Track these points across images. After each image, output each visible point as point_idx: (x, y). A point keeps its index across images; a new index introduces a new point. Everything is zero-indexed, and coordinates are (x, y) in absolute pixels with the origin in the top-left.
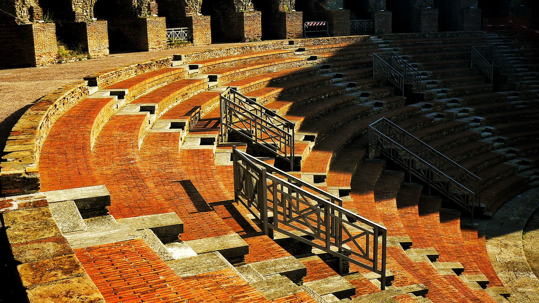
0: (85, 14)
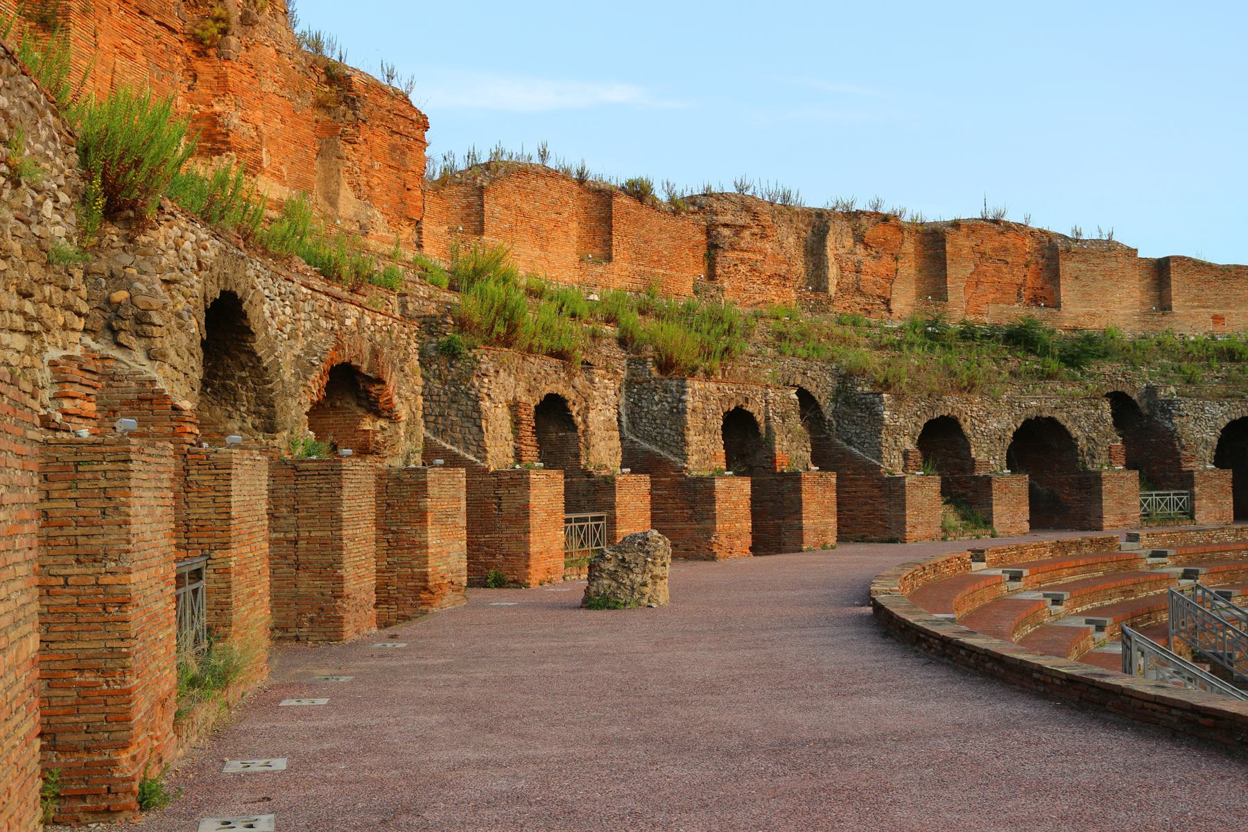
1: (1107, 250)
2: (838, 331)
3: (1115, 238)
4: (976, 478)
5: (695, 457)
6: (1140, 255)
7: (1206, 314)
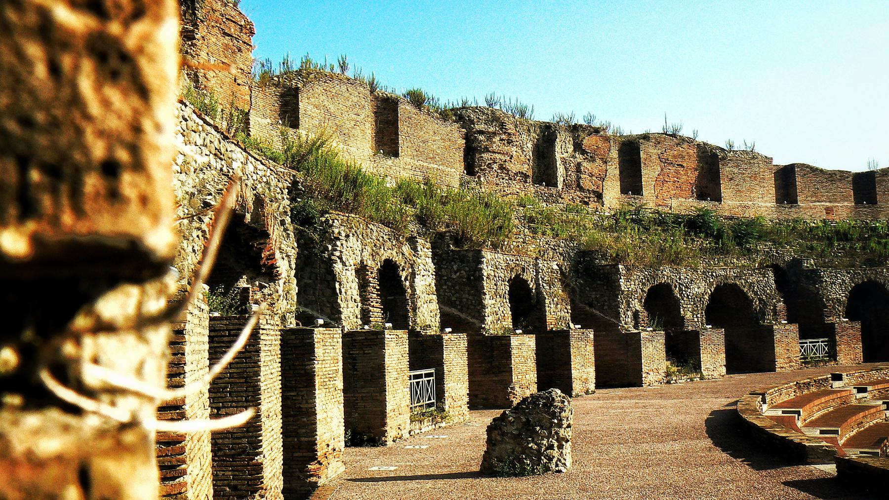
0: (696, 320)
1: (751, 157)
3: (756, 150)
4: (688, 332)
6: (774, 163)
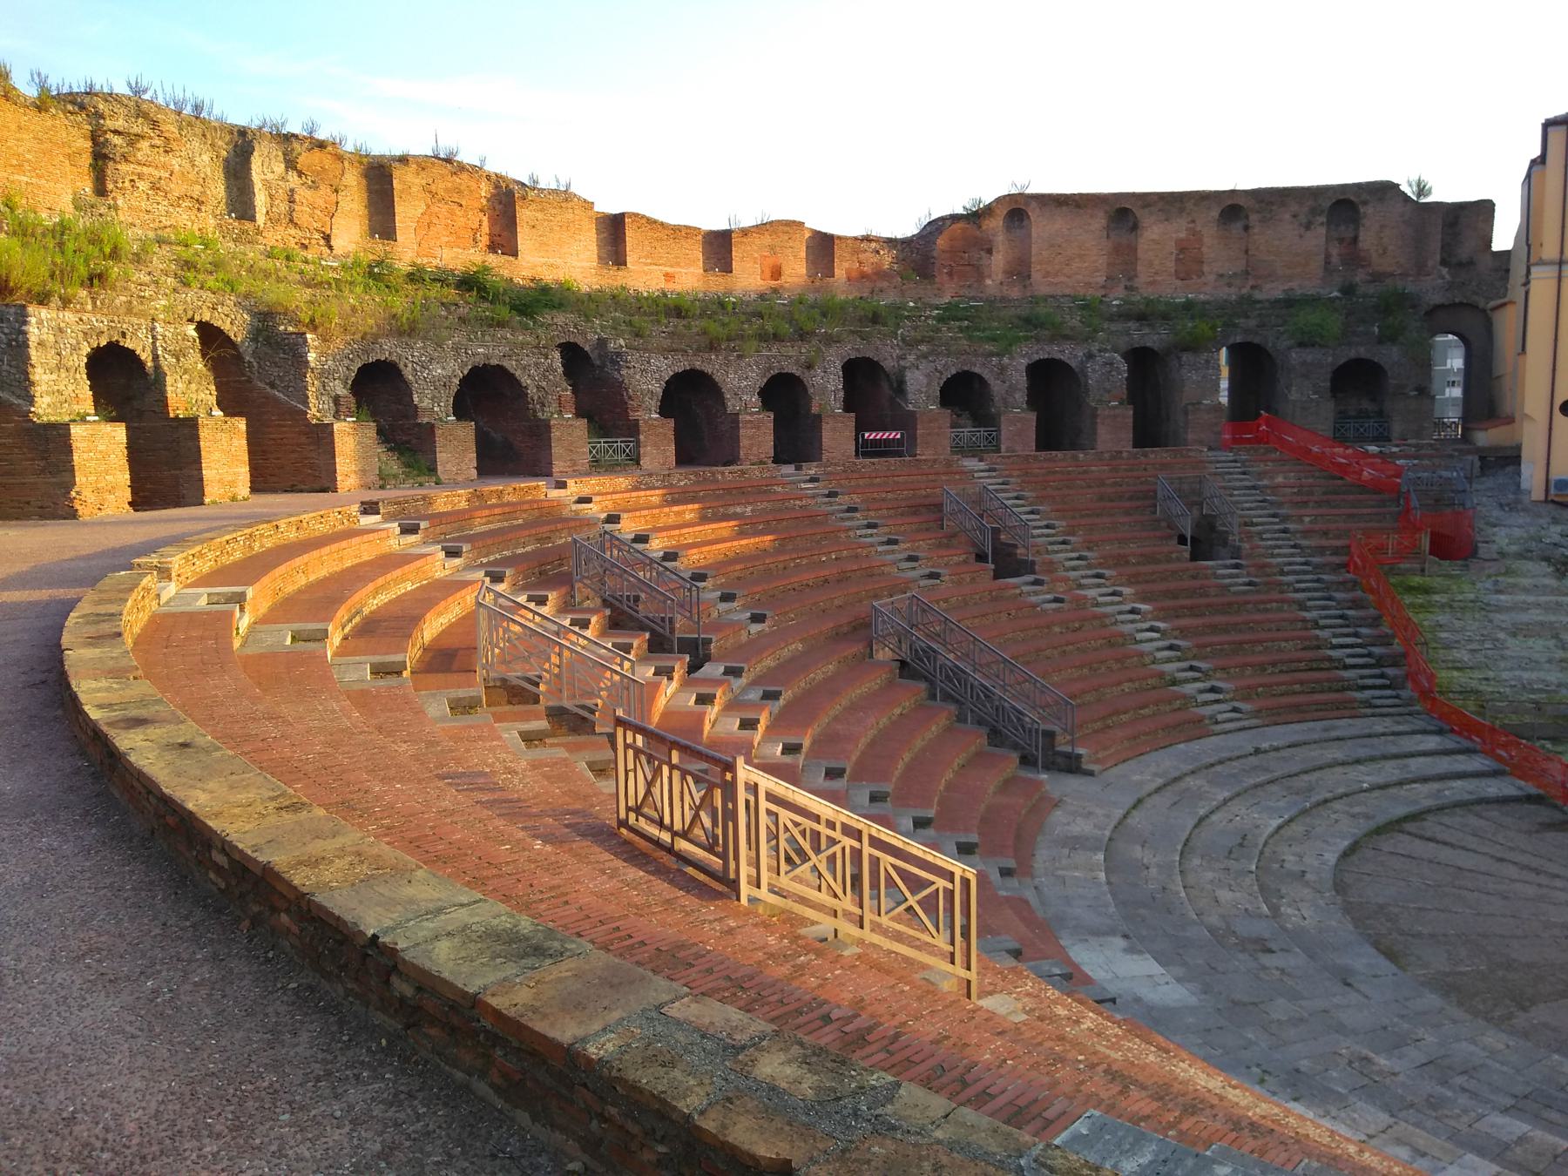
1: (564, 197)
2: (269, 264)
3: (573, 189)
5: (47, 399)
6: (596, 209)
7: (657, 271)
